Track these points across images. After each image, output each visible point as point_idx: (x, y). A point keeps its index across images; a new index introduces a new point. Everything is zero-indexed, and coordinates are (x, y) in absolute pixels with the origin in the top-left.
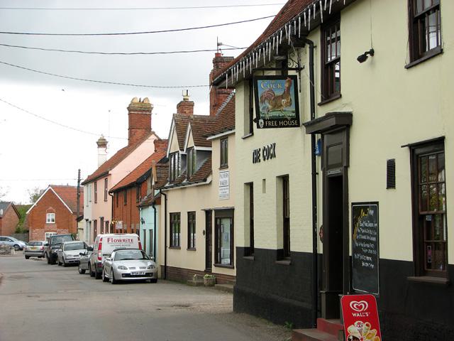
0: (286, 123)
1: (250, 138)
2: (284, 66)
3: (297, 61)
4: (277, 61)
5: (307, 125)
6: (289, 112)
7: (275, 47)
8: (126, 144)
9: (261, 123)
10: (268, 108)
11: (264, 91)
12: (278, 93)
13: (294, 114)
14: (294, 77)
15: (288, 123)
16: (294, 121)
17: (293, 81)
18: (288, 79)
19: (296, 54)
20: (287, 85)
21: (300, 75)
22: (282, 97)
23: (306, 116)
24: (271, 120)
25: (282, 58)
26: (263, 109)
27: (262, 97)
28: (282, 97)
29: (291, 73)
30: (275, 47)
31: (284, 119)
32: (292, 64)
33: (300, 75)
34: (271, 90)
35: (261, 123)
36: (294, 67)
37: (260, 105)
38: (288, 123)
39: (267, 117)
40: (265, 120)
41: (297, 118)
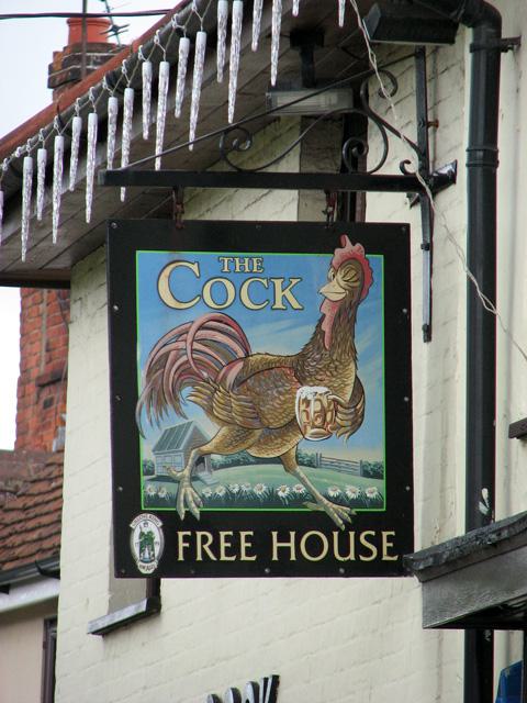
0: (314, 546)
1: (141, 634)
2: (346, 182)
3: (412, 133)
4: (312, 124)
5: (441, 567)
6: (342, 470)
7: (266, 36)
8: (143, 608)
9: (147, 540)
10: (198, 439)
11: (175, 322)
12: (275, 340)
13: (375, 489)
14: (392, 240)
15: (329, 545)
16: (376, 538)
17: (377, 262)
18: (349, 248)
19: (409, 82)
20: (335, 290)
21: (429, 219)
22: (299, 369)
23: (440, 515)
24: (211, 521)
25: (324, 102)
26: (167, 443)
27: (158, 365)
28: (299, 369)
29: (383, 208)
30: (266, 36)
31: (302, 518)
32: (389, 154)
33: (429, 219)
34: (224, 321)
35: (147, 540)
36: (391, 169)
37: (145, 418)
38: (329, 545)
39: (191, 499)
40: (171, 523)
41: (397, 510)
